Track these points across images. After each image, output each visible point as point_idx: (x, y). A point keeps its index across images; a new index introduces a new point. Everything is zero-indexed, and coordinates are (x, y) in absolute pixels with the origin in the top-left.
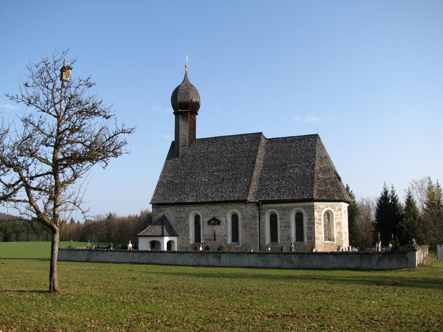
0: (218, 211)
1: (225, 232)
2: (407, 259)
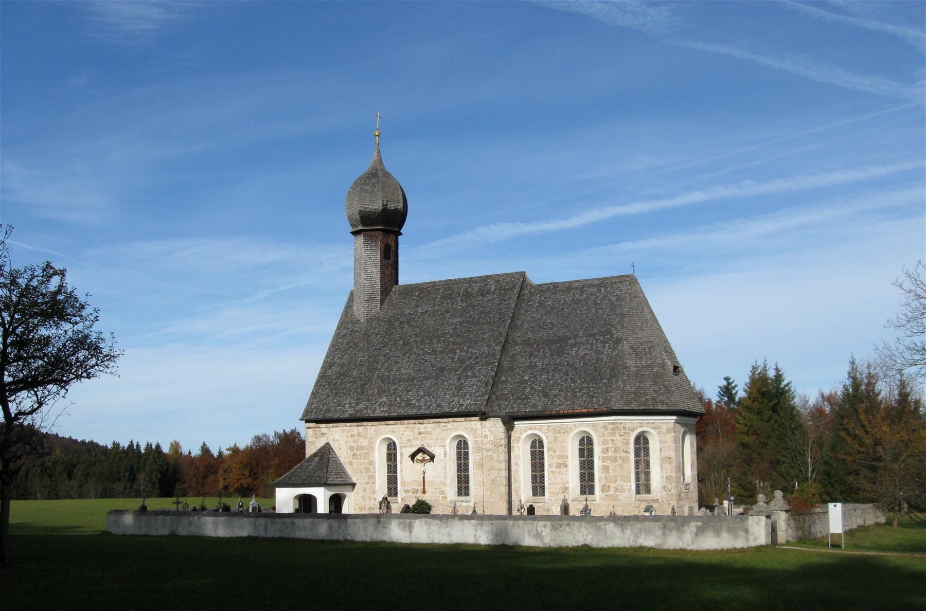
0: (429, 433)
1: (443, 475)
2: (747, 531)
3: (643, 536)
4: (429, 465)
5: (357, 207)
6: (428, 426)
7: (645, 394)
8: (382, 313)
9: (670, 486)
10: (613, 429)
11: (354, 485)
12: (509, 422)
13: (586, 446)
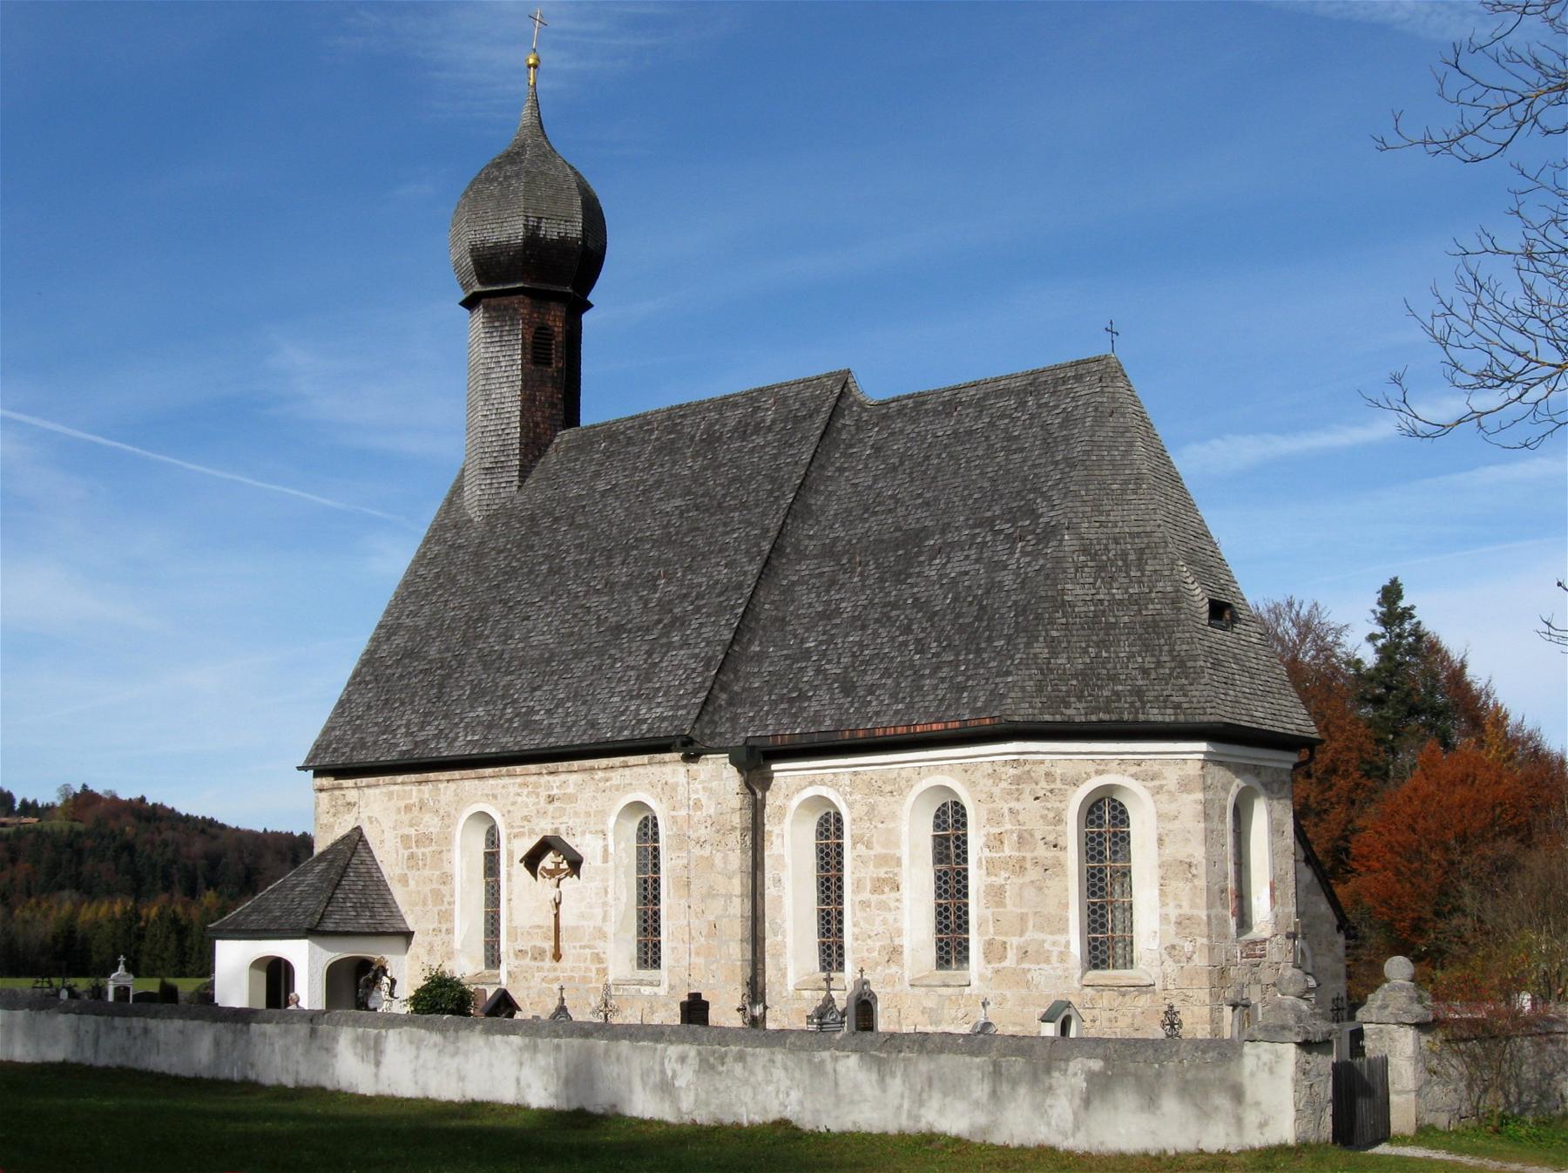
0: (571, 798)
1: (599, 911)
2: (1237, 1094)
3: (935, 1101)
4: (569, 883)
5: (470, 236)
6: (569, 779)
7: (1113, 678)
8: (520, 499)
9: (1188, 947)
10: (1017, 780)
11: (408, 935)
12: (756, 763)
13: (950, 829)
